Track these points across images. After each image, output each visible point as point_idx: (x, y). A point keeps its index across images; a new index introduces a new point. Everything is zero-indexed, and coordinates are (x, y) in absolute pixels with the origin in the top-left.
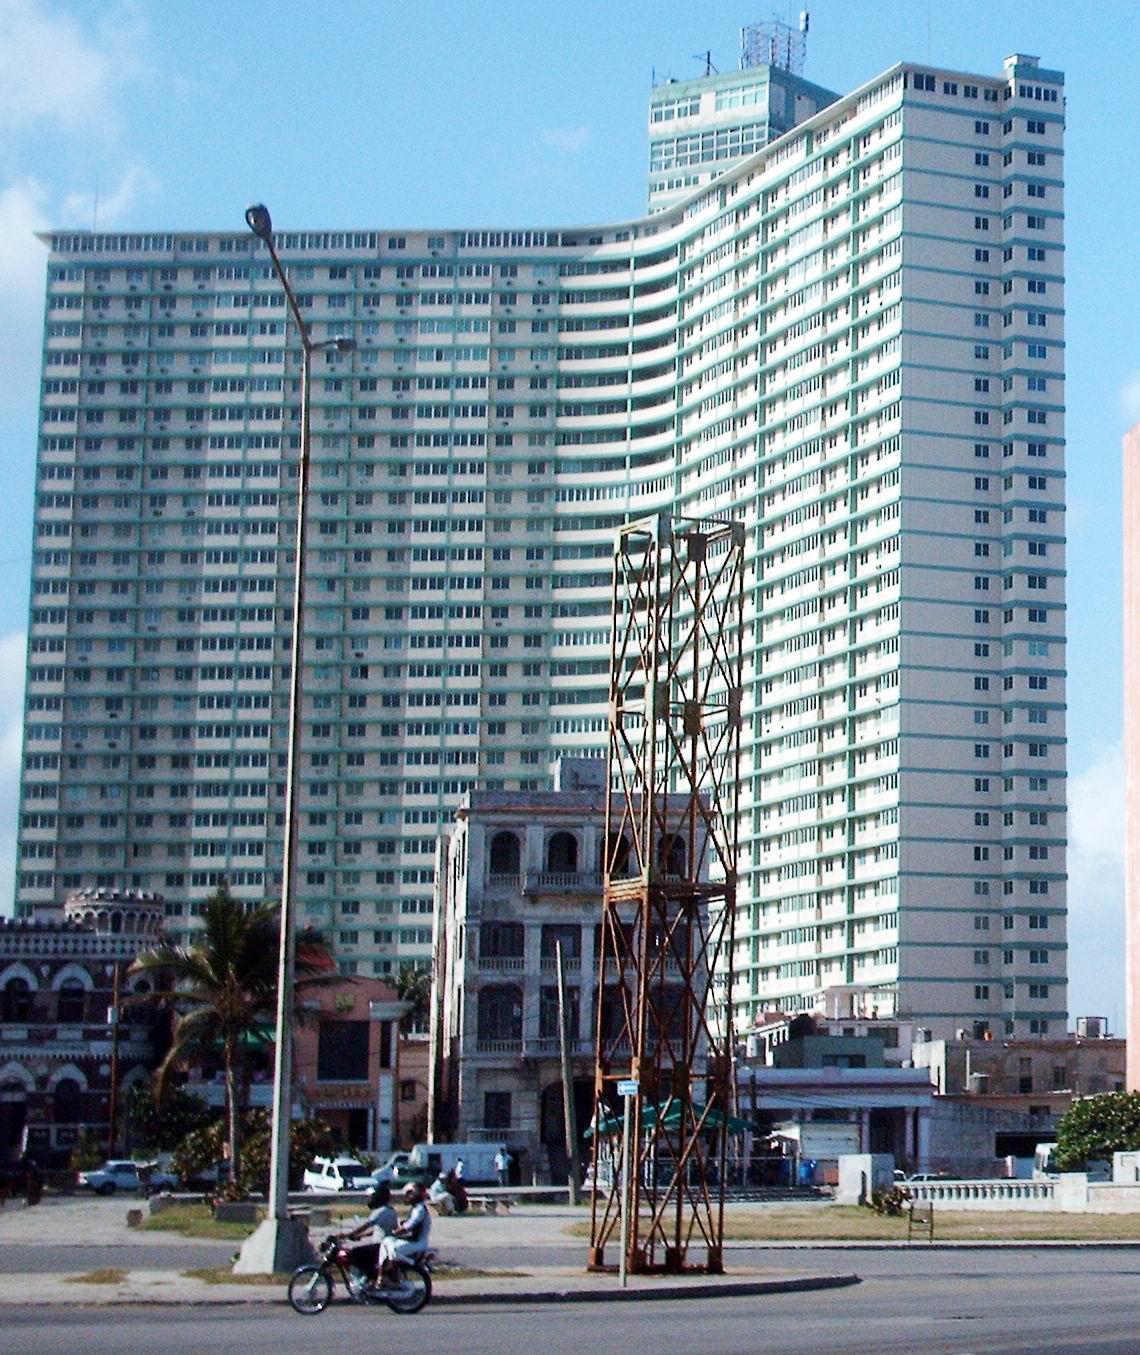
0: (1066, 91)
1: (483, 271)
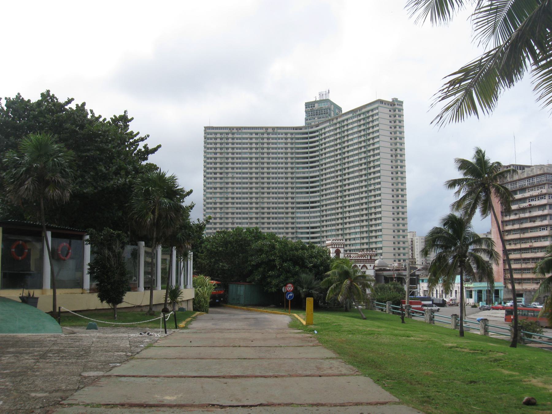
0: (404, 105)
1: (282, 134)
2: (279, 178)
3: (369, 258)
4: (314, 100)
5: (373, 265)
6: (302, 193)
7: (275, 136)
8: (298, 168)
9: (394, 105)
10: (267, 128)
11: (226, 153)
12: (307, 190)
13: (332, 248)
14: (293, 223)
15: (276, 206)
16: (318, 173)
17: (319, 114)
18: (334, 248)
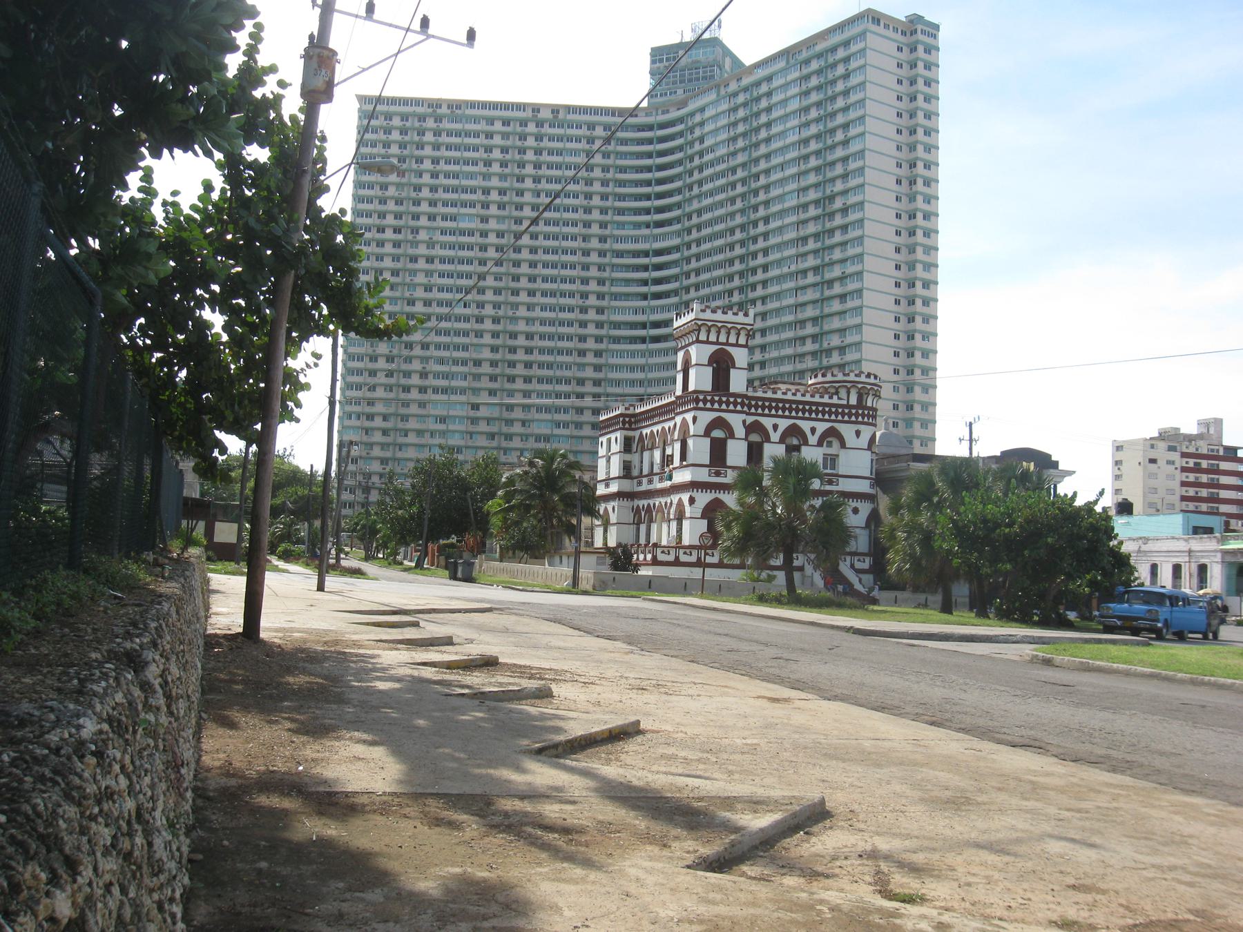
0: (942, 35)
1: (579, 127)
2: (565, 252)
3: (853, 400)
4: (676, 40)
5: (866, 432)
6: (627, 296)
7: (560, 131)
8: (621, 225)
9: (913, 32)
10: (536, 108)
11: (415, 171)
12: (644, 289)
13: (698, 341)
14: (597, 383)
15: (457, 154)
16: (676, 241)
17: (690, 80)
18: (707, 342)
